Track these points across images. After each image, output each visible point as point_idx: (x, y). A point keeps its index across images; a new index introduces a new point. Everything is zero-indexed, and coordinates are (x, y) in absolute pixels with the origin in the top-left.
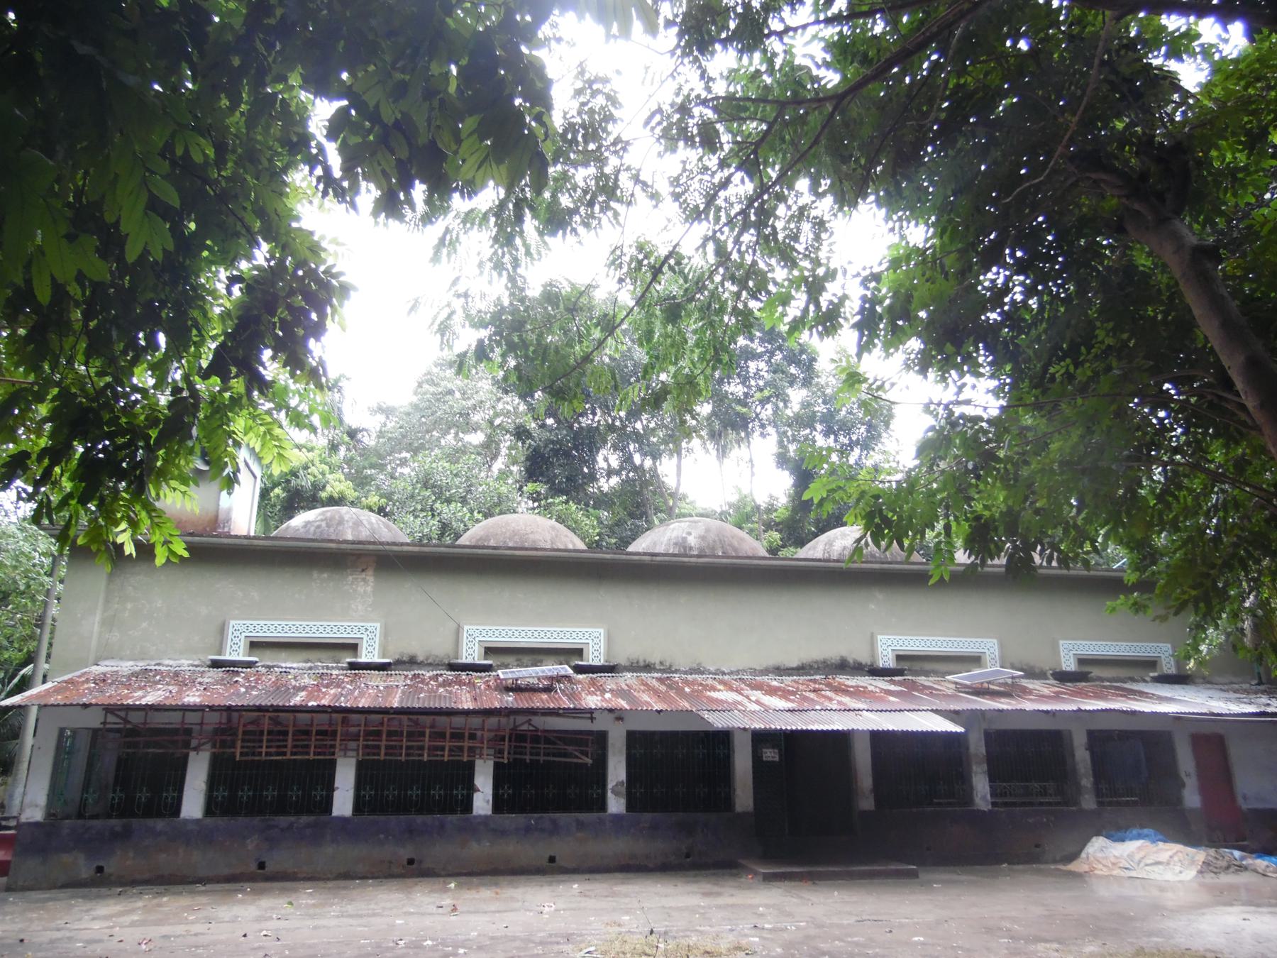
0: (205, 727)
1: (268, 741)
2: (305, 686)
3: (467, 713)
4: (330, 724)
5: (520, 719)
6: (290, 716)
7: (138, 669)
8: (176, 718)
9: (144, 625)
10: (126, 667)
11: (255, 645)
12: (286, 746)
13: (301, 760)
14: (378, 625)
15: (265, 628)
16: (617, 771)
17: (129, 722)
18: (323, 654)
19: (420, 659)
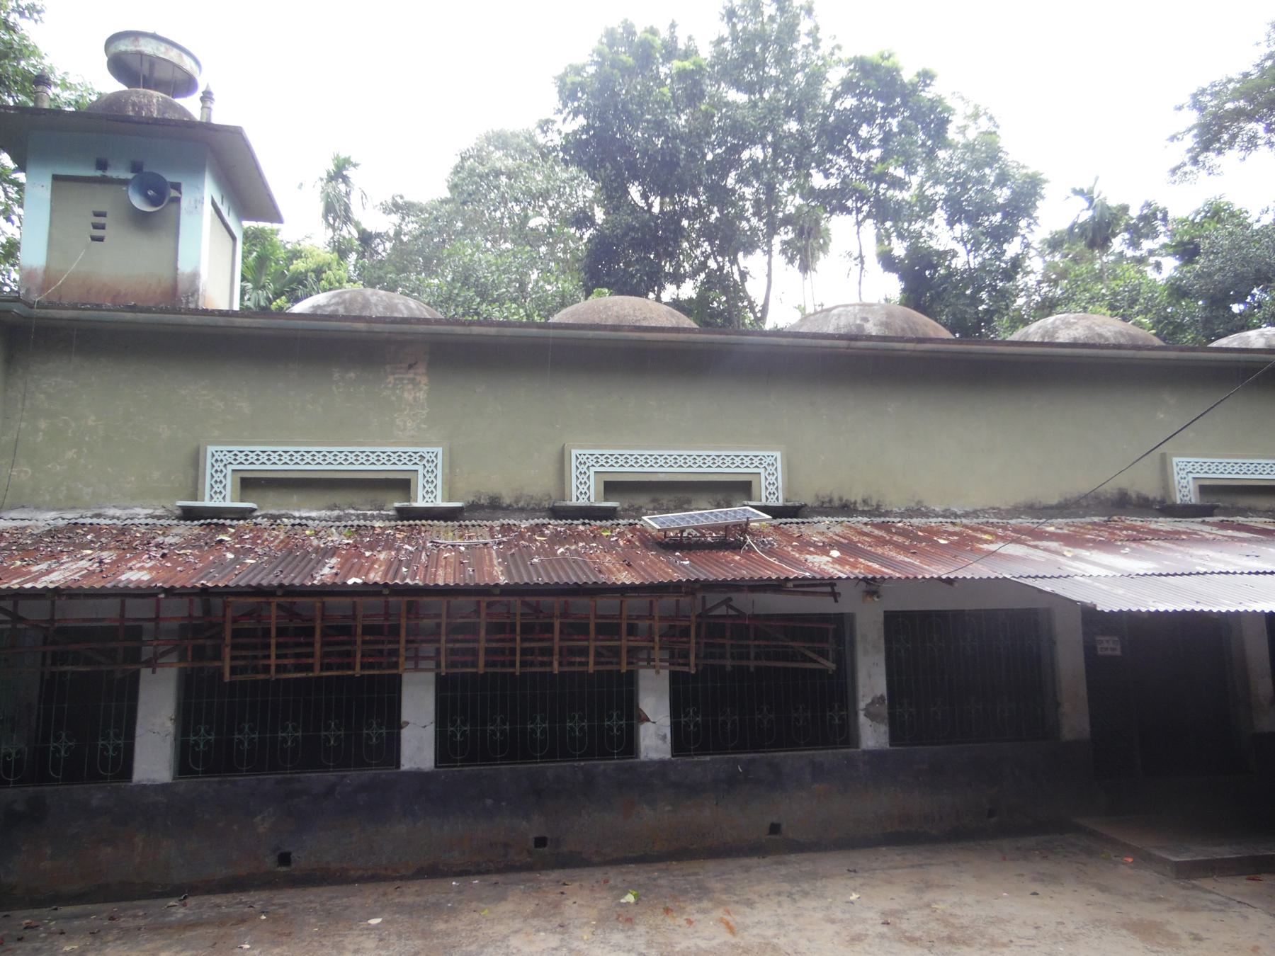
0: (164, 625)
1: (278, 646)
2: (338, 554)
3: (624, 590)
4: (387, 615)
5: (713, 599)
6: (317, 602)
7: (61, 523)
8: (108, 611)
9: (70, 454)
10: (46, 519)
11: (248, 484)
12: (311, 655)
13: (338, 677)
14: (439, 450)
15: (263, 458)
16: (871, 680)
17: (22, 619)
18: (357, 497)
19: (507, 501)
